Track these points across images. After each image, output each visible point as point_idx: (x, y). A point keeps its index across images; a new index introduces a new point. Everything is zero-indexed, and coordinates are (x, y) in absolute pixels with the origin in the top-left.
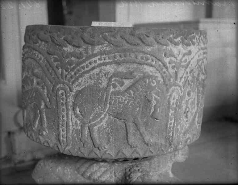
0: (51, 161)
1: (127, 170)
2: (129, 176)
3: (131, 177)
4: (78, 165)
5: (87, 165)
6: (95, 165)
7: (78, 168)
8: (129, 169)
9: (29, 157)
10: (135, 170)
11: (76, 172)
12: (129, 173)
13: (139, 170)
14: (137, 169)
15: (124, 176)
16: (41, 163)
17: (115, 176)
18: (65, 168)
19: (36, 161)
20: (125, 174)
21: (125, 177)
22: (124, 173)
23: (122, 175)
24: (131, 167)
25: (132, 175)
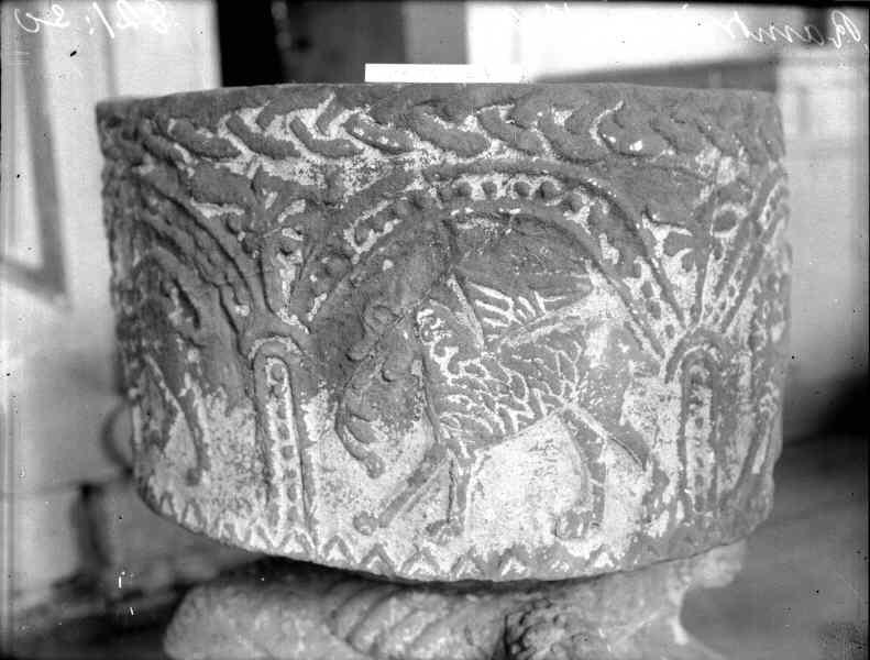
0: (230, 590)
1: (513, 621)
2: (520, 641)
3: (526, 644)
4: (331, 604)
5: (363, 604)
6: (393, 601)
7: (334, 615)
8: (520, 614)
9: (161, 577)
10: (542, 621)
11: (325, 630)
12: (521, 630)
13: (555, 620)
14: (549, 615)
15: (502, 645)
16: (198, 599)
17: (470, 642)
18: (286, 614)
19: (182, 589)
20: (506, 633)
21: (507, 648)
22: (503, 630)
23: (496, 636)
24: (528, 608)
25: (532, 636)
